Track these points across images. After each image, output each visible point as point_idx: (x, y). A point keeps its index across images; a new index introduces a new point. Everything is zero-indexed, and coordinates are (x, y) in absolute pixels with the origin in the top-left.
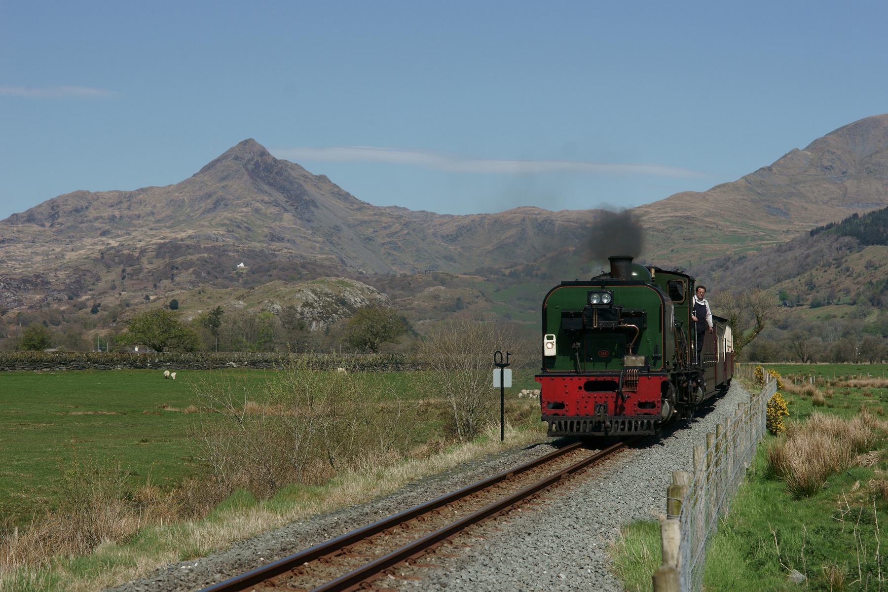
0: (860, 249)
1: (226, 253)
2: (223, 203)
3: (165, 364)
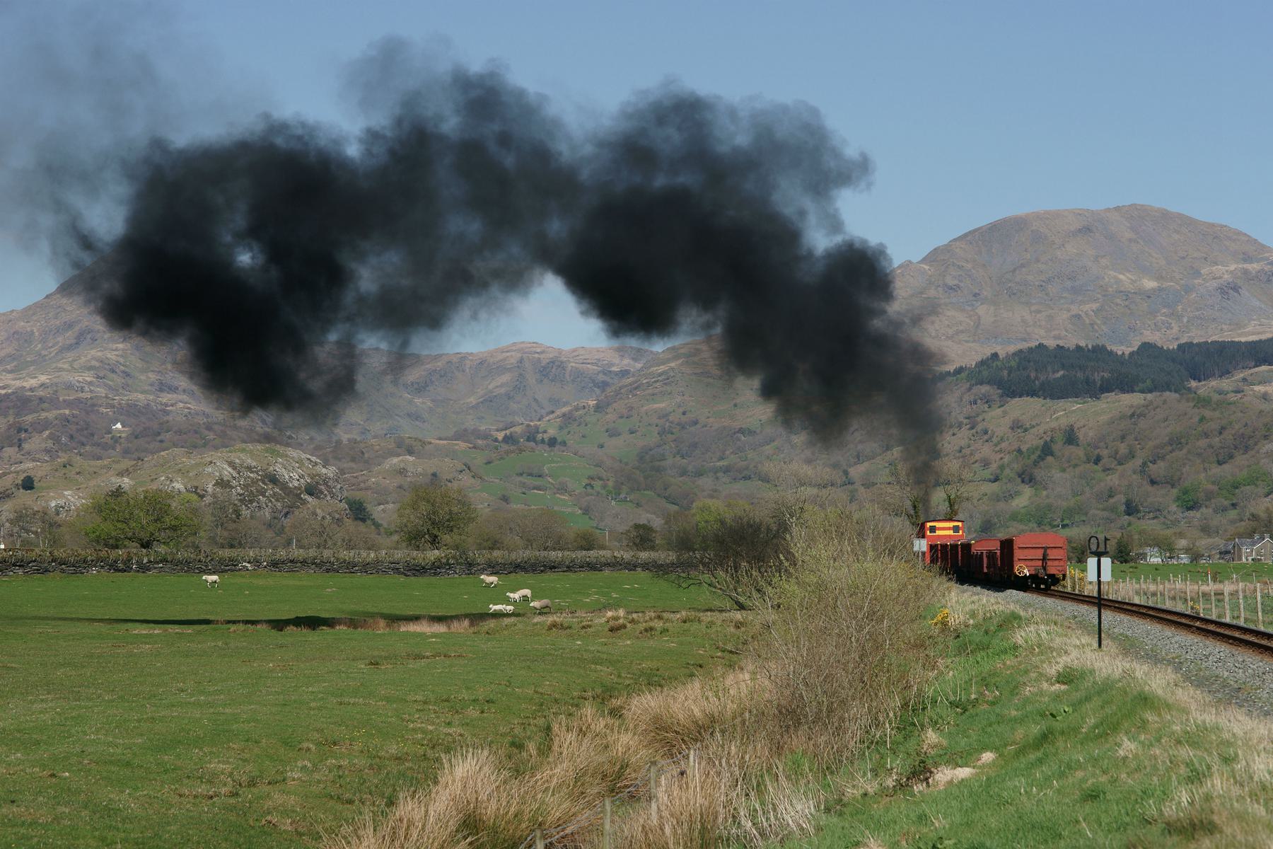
0: (1002, 403)
1: (96, 408)
2: (89, 336)
3: (156, 566)
